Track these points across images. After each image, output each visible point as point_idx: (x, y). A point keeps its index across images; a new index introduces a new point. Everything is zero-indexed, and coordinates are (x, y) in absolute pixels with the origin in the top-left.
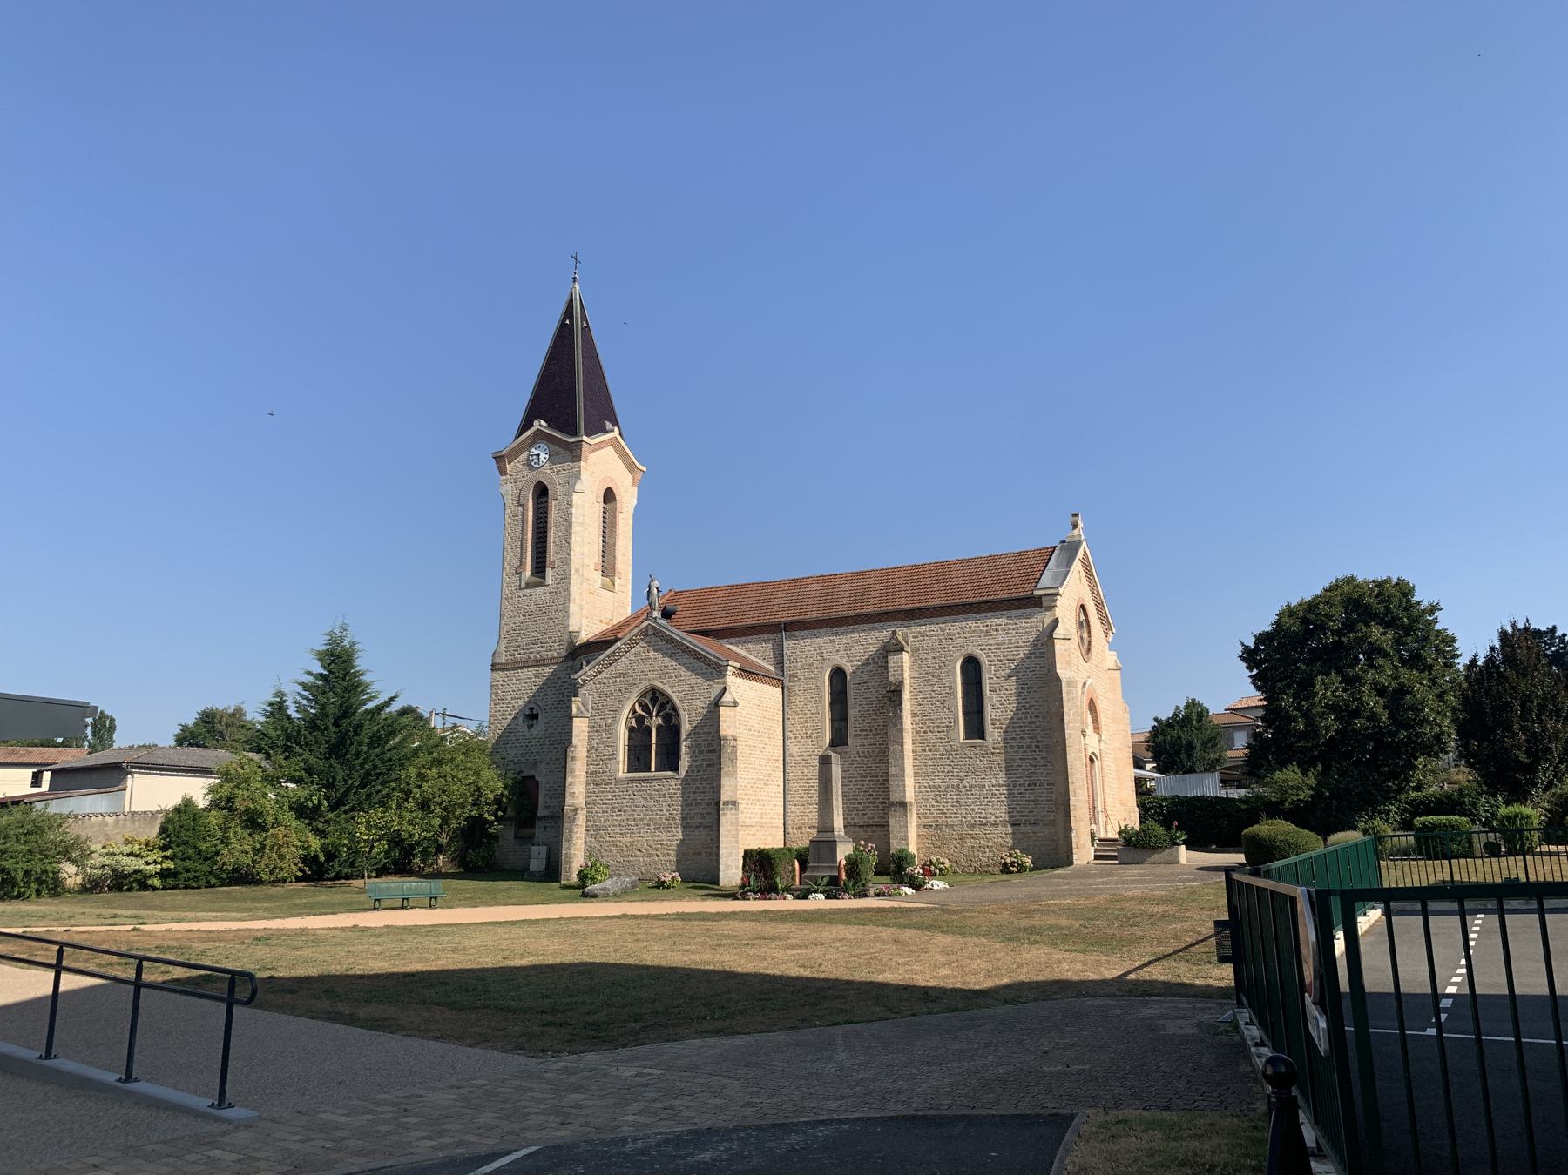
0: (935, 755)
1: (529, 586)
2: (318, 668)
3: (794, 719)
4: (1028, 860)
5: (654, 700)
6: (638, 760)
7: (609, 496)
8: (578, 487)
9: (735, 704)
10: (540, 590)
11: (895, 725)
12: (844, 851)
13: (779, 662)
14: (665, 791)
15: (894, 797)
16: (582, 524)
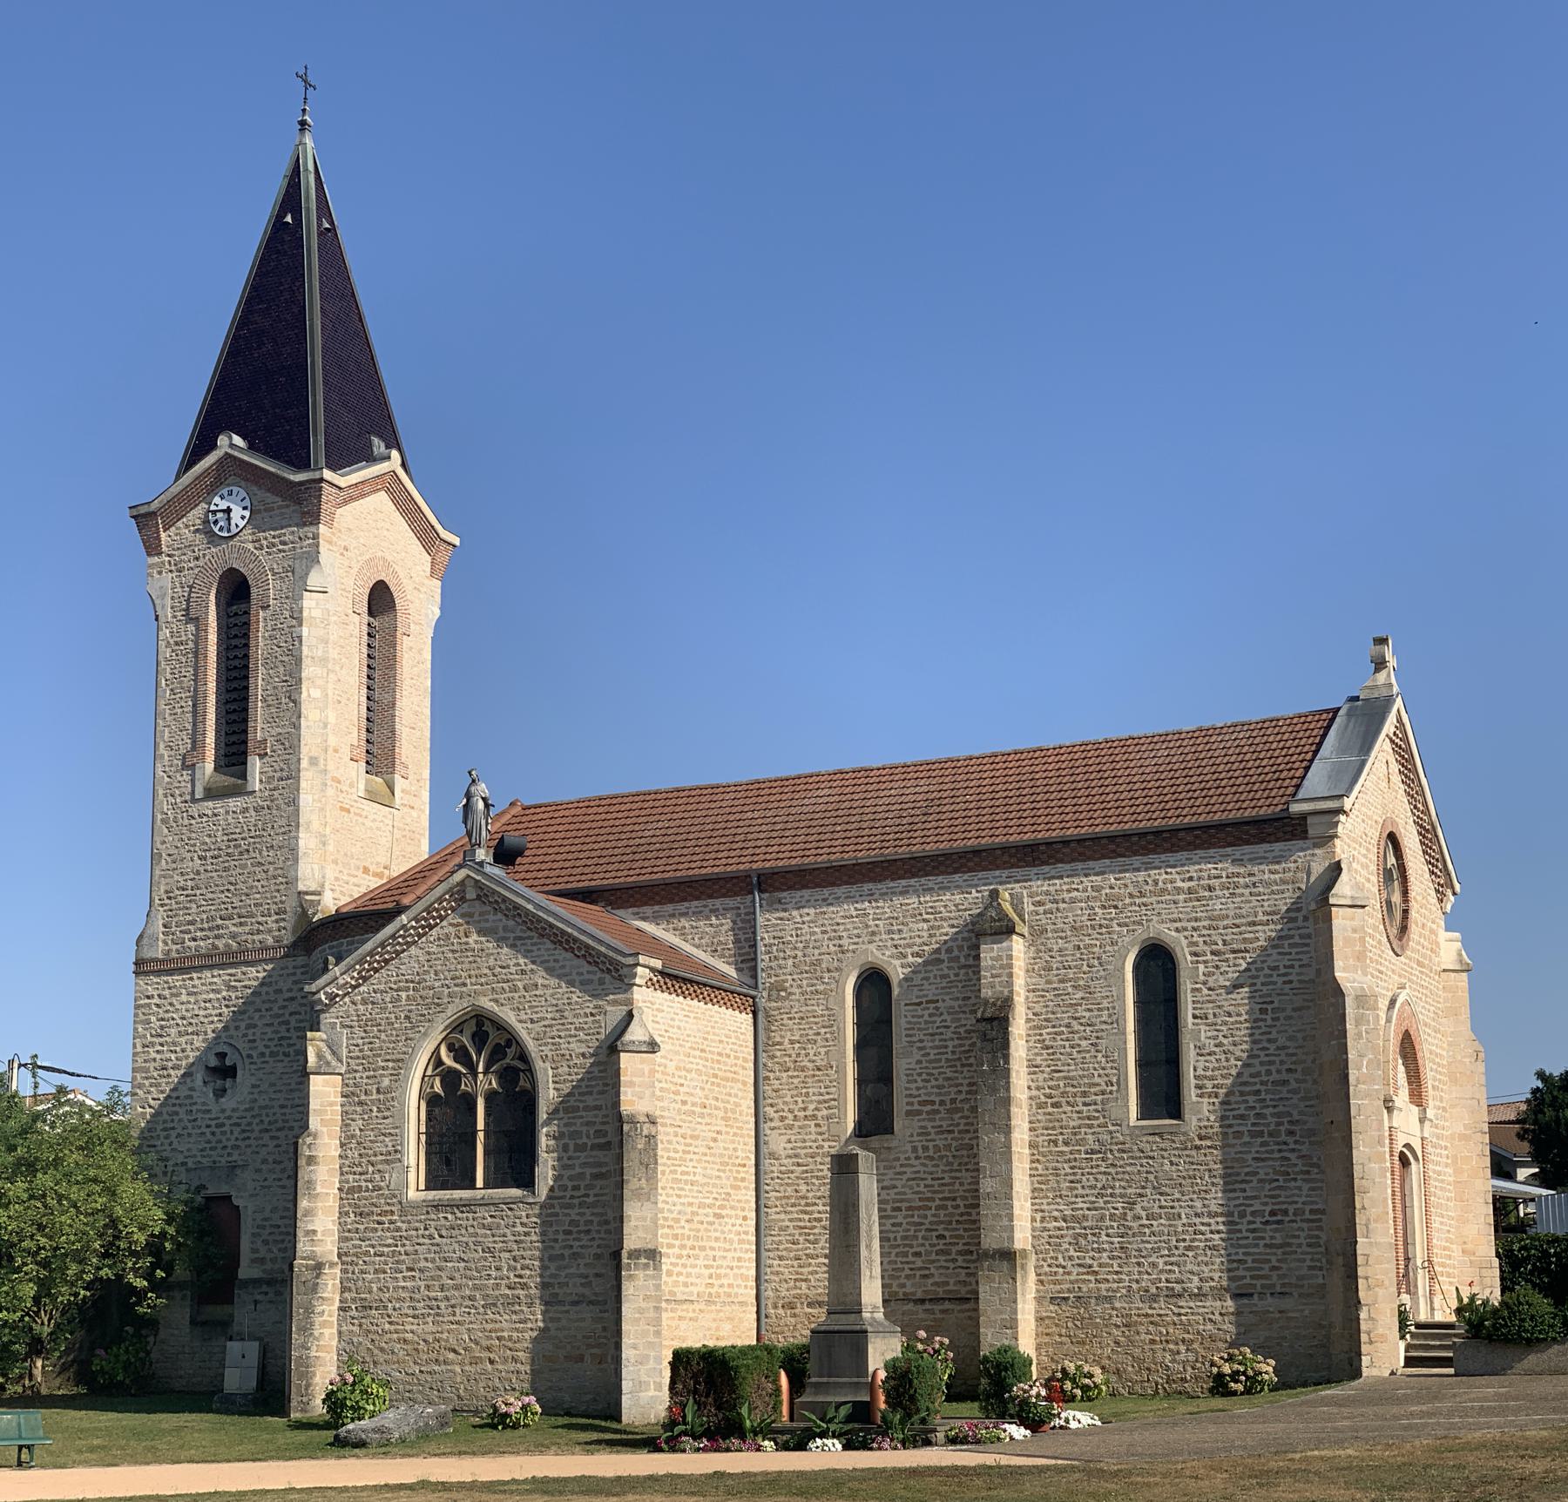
0: (1061, 1155)
1: (212, 794)
3: (778, 1080)
4: (1267, 1368)
5: (480, 1038)
6: (448, 1163)
7: (380, 600)
8: (314, 580)
9: (653, 1047)
10: (235, 803)
11: (994, 1090)
12: (882, 1352)
13: (747, 959)
14: (504, 1229)
15: (989, 1241)
16: (324, 661)
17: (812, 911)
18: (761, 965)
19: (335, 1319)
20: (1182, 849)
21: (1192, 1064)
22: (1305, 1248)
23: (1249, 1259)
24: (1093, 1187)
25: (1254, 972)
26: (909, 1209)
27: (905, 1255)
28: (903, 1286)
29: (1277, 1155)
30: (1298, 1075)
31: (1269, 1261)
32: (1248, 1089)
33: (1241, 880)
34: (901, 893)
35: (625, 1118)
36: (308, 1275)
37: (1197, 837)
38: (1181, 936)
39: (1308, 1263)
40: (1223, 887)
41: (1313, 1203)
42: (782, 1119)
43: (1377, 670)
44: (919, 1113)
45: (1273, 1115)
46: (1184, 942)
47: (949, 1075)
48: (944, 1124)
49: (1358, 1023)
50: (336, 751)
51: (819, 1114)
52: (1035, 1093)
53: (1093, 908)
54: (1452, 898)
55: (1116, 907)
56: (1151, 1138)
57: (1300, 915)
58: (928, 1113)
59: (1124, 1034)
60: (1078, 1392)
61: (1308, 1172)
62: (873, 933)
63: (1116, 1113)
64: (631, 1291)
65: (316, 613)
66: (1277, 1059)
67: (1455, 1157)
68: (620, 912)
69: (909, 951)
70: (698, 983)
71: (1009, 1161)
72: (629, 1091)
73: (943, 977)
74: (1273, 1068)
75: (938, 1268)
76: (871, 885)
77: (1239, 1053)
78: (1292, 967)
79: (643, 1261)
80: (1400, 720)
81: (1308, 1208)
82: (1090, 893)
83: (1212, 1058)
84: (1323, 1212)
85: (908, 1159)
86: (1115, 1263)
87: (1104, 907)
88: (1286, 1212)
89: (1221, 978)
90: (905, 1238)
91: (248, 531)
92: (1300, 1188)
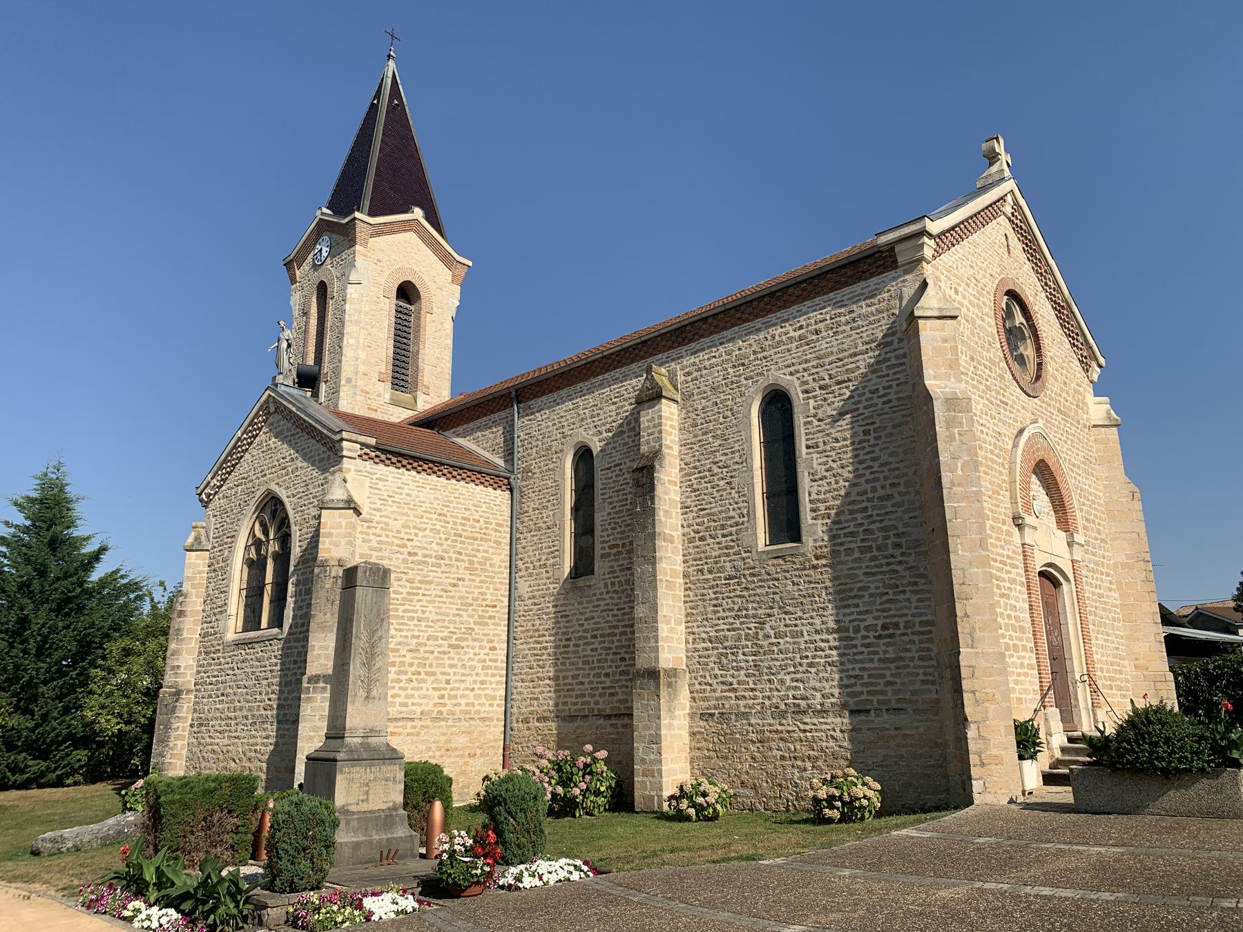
0: (715, 579)
2: (20, 519)
3: (527, 539)
7: (407, 292)
11: (644, 528)
15: (642, 662)
16: (358, 322)
18: (516, 456)
19: (186, 733)
20: (793, 303)
21: (807, 488)
22: (917, 662)
23: (865, 674)
24: (731, 610)
25: (856, 399)
26: (602, 636)
27: (599, 675)
28: (597, 703)
29: (885, 569)
30: (902, 489)
31: (884, 676)
33: (843, 319)
36: (169, 700)
37: (803, 290)
38: (794, 378)
39: (921, 677)
40: (829, 328)
41: (921, 615)
42: (527, 568)
43: (991, 164)
44: (609, 555)
45: (878, 529)
46: (797, 383)
47: (629, 522)
48: (625, 562)
49: (949, 425)
52: (687, 530)
55: (743, 365)
56: (775, 562)
57: (895, 338)
58: (615, 555)
60: (692, 811)
61: (916, 583)
63: (746, 541)
64: (308, 712)
66: (881, 476)
68: (446, 433)
70: (433, 462)
71: (655, 588)
72: (327, 540)
73: (625, 444)
74: (877, 484)
75: (620, 687)
76: (581, 384)
77: (846, 475)
78: (890, 387)
79: (322, 685)
80: (1016, 203)
81: (918, 620)
82: (725, 357)
83: (823, 482)
84: (932, 623)
85: (602, 594)
86: (750, 680)
87: (734, 366)
88: (896, 625)
89: (829, 409)
92: (908, 600)
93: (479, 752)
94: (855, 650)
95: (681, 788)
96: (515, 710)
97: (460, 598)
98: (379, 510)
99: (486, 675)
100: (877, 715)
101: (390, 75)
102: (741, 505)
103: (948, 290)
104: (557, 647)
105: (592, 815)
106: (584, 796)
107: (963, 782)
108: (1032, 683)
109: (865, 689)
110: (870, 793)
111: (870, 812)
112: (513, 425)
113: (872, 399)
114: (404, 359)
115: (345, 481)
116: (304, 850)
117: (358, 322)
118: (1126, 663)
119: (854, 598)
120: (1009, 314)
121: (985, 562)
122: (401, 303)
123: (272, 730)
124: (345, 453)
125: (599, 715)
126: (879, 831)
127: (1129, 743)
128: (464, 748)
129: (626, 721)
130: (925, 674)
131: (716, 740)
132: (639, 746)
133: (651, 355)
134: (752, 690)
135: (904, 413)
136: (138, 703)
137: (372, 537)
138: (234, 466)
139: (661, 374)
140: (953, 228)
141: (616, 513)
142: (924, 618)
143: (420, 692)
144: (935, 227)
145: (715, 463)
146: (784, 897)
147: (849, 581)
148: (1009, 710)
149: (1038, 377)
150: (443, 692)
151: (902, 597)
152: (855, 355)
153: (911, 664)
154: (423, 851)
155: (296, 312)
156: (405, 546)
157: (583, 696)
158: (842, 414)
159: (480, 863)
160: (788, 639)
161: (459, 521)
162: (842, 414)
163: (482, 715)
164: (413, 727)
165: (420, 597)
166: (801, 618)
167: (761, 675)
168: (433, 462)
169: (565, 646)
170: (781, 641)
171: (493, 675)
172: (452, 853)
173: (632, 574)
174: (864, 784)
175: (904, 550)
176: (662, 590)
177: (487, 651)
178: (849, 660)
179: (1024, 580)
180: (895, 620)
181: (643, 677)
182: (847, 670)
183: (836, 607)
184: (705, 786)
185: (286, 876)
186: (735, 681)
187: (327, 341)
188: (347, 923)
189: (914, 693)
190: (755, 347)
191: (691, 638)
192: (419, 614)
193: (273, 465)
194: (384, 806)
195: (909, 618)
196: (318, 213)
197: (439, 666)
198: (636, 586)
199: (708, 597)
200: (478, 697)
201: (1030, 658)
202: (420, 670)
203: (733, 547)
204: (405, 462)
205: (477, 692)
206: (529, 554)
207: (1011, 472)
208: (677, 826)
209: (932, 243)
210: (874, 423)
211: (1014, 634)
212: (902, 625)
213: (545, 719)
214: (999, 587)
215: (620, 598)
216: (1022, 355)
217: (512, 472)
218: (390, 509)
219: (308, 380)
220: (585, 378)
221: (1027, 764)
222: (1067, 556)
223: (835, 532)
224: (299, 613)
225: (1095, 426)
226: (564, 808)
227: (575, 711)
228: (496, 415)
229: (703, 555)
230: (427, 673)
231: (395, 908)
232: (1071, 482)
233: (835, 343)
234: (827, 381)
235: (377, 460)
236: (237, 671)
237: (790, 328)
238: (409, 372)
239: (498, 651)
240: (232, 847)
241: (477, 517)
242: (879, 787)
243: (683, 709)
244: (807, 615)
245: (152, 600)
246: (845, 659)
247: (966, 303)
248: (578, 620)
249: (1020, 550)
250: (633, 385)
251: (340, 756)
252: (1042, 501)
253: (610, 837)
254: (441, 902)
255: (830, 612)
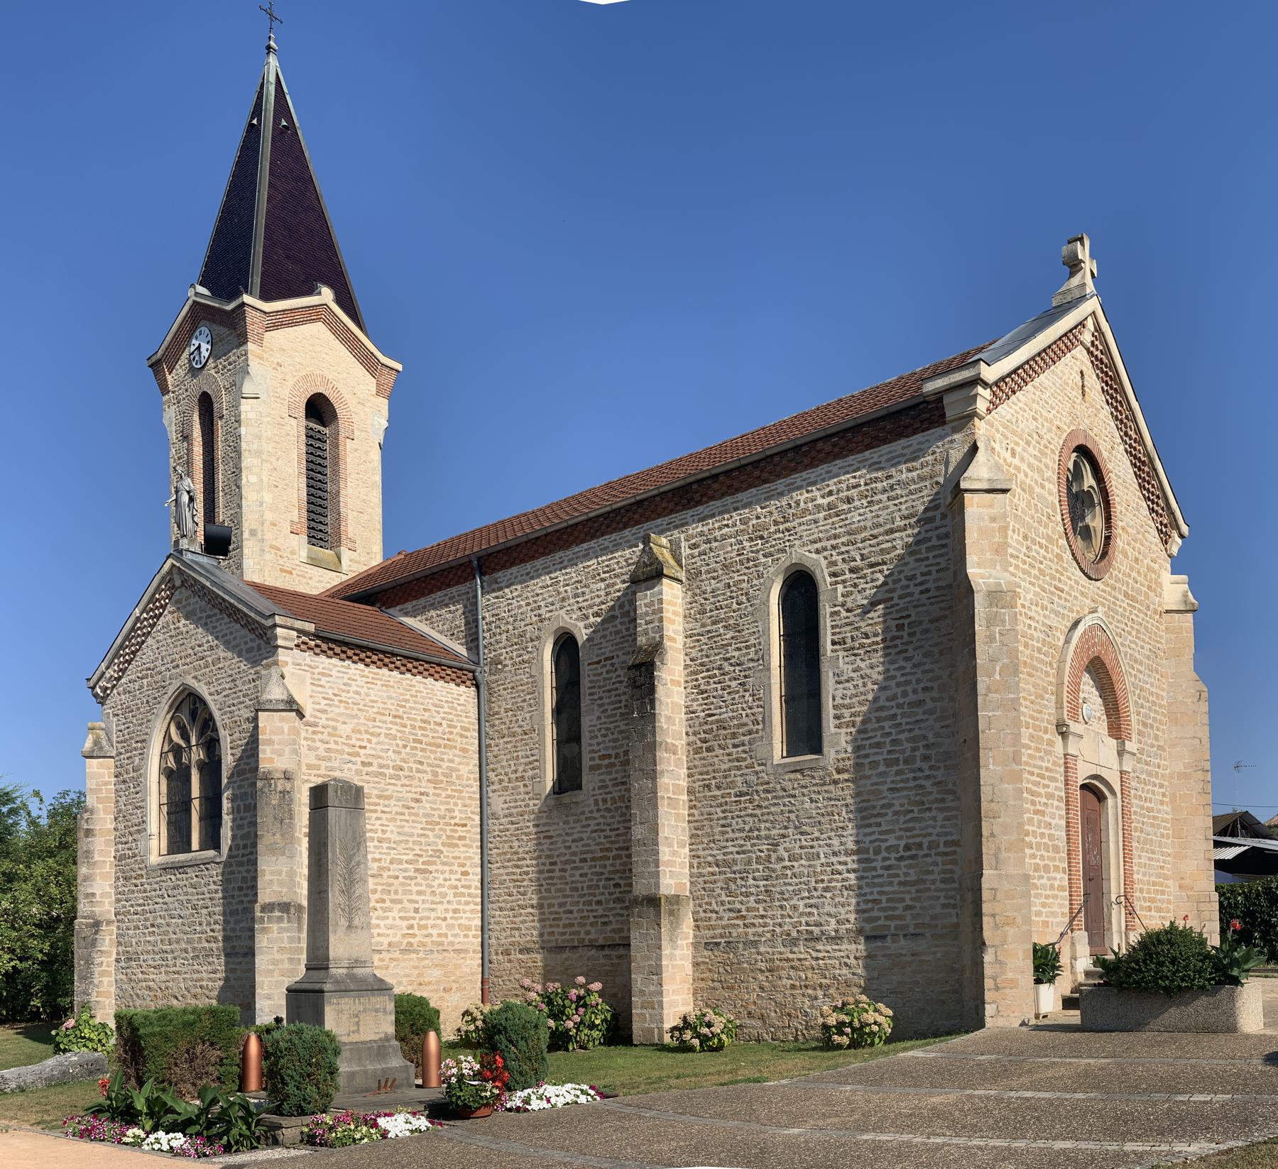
3: (499, 746)
7: (319, 410)
8: (248, 388)
11: (643, 736)
15: (640, 889)
16: (258, 453)
17: (519, 587)
18: (482, 643)
19: (112, 969)
20: (822, 462)
22: (939, 885)
23: (884, 898)
24: (742, 830)
25: (891, 586)
26: (593, 859)
28: (588, 933)
29: (912, 784)
30: (935, 694)
32: (884, 714)
33: (879, 485)
34: (584, 556)
35: (260, 775)
36: (87, 932)
37: (834, 445)
38: (820, 557)
39: (942, 901)
40: (862, 496)
41: (946, 834)
43: (1072, 275)
46: (824, 563)
47: (623, 728)
48: (618, 776)
49: (989, 623)
50: (274, 525)
51: (526, 775)
52: (692, 738)
53: (741, 542)
54: (1180, 541)
55: (762, 538)
56: (792, 776)
57: (938, 513)
58: (607, 767)
59: (769, 669)
60: (696, 1042)
61: (943, 800)
62: (563, 599)
64: (265, 943)
65: (251, 415)
66: (913, 678)
67: (1173, 796)
68: (391, 611)
69: (590, 611)
70: (384, 652)
72: (268, 749)
73: (617, 633)
74: (909, 688)
75: (615, 915)
76: (561, 554)
77: (876, 676)
78: (929, 573)
79: (277, 914)
80: (1098, 328)
81: (942, 840)
83: (849, 685)
85: (591, 812)
86: (761, 907)
87: (751, 539)
88: (920, 846)
89: (859, 597)
90: (590, 887)
91: (211, 361)
92: (934, 818)
93: (454, 986)
94: (874, 873)
95: (685, 1019)
96: (493, 941)
97: (425, 815)
98: (324, 711)
99: (459, 903)
100: (894, 941)
101: (272, 79)
102: (755, 710)
103: (1003, 452)
104: (540, 872)
105: (586, 1048)
106: (578, 1029)
107: (977, 1007)
108: (1061, 906)
109: (882, 914)
110: (881, 1019)
111: (880, 1037)
112: (476, 604)
113: (908, 586)
114: (320, 501)
115: (283, 677)
116: (309, 1076)
117: (258, 453)
118: (1170, 883)
119: (876, 816)
120: (1077, 474)
121: (1017, 777)
122: (312, 425)
123: (219, 963)
124: (280, 642)
125: (591, 946)
126: (887, 1054)
127: (1137, 963)
128: (438, 982)
129: (622, 951)
130: (946, 897)
131: (721, 970)
132: (637, 979)
133: (648, 519)
134: (762, 917)
135: (943, 605)
136: (32, 935)
137: (318, 744)
138: (134, 653)
139: (661, 545)
140: (1015, 371)
141: (608, 717)
142: (949, 838)
143: (387, 922)
144: (990, 373)
145: (726, 659)
146: (786, 1109)
147: (871, 797)
148: (1030, 933)
149: (1104, 554)
150: (411, 922)
151: (927, 814)
152: (891, 531)
153: (933, 887)
154: (420, 1082)
155: (173, 436)
156: (358, 755)
157: (572, 925)
158: (873, 604)
159: (489, 1085)
160: (803, 862)
161: (417, 724)
162: (873, 604)
163: (458, 947)
164: (381, 960)
165: (379, 815)
166: (818, 839)
167: (772, 900)
168: (384, 652)
169: (549, 871)
170: (795, 864)
171: (467, 903)
172: (461, 1077)
173: (628, 790)
174: (876, 1010)
175: (933, 763)
176: (663, 808)
177: (459, 876)
178: (867, 884)
179: (1063, 794)
180: (918, 840)
181: (642, 905)
182: (865, 895)
183: (858, 827)
184: (711, 1016)
185: (293, 1100)
186: (744, 908)
187: (220, 478)
188: (366, 1140)
189: (934, 917)
190: (776, 516)
191: (695, 862)
192: (380, 834)
193: (184, 652)
194: (376, 1037)
195: (934, 838)
196: (191, 293)
197: (405, 892)
198: (633, 804)
199: (715, 817)
200: (450, 927)
201: (1062, 879)
202: (385, 897)
203: (745, 759)
204: (350, 653)
205: (450, 921)
206: (502, 764)
207: (1060, 672)
208: (681, 1056)
209: (987, 393)
210: (909, 616)
211: (1046, 854)
212: (925, 846)
213: (528, 951)
214: (1033, 803)
215: (613, 817)
216: (1087, 528)
217: (478, 664)
218: (337, 710)
219: (219, 544)
220: (566, 545)
221: (1044, 988)
222: (1116, 766)
223: (859, 743)
224: (240, 833)
225: (1167, 612)
226: (559, 1041)
227: (563, 941)
228: (454, 590)
229: (710, 768)
230: (392, 901)
231: (410, 1127)
232: (1129, 680)
233: (870, 515)
234: (859, 563)
235: (317, 650)
236: (167, 899)
237: (817, 494)
238: (328, 520)
239: (471, 876)
240: (219, 1078)
241: (438, 720)
242: (890, 1013)
243: (687, 938)
244: (825, 836)
245: (29, 814)
246: (863, 883)
247: (1024, 467)
248: (564, 841)
249: (1062, 761)
250: (624, 558)
251: (327, 987)
252: (1093, 703)
253: (609, 1067)
254: (451, 1123)
255: (850, 832)
